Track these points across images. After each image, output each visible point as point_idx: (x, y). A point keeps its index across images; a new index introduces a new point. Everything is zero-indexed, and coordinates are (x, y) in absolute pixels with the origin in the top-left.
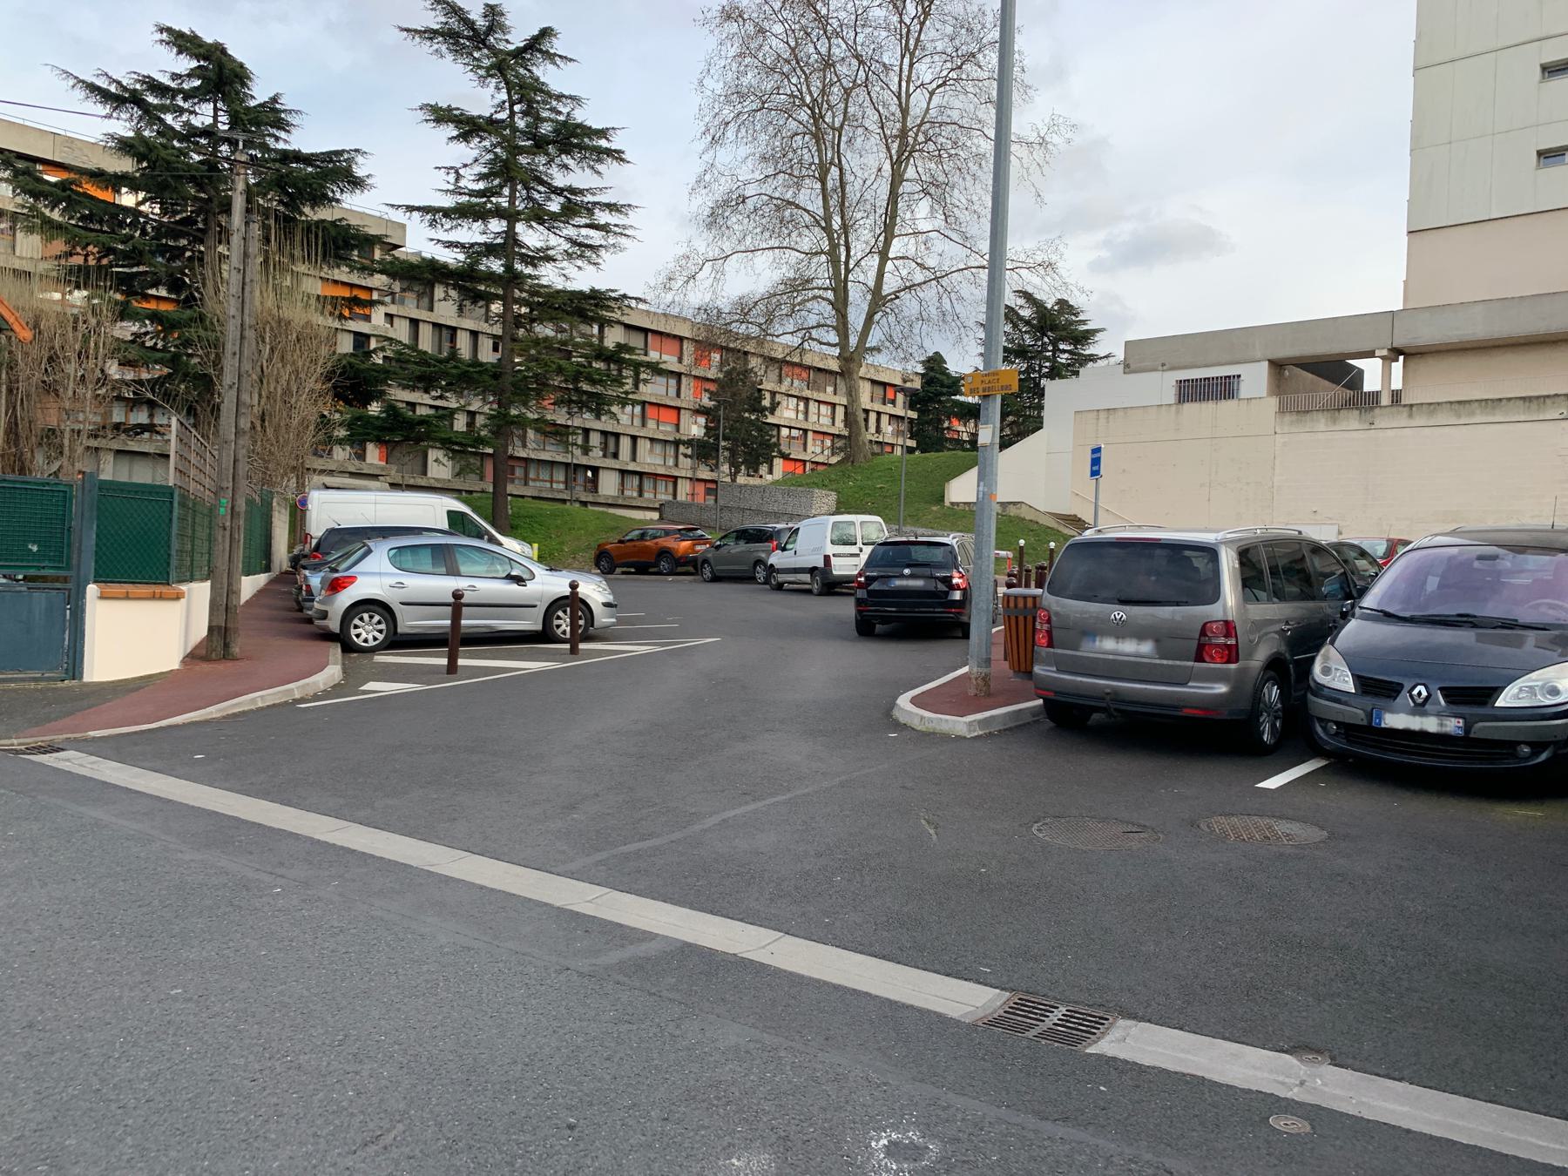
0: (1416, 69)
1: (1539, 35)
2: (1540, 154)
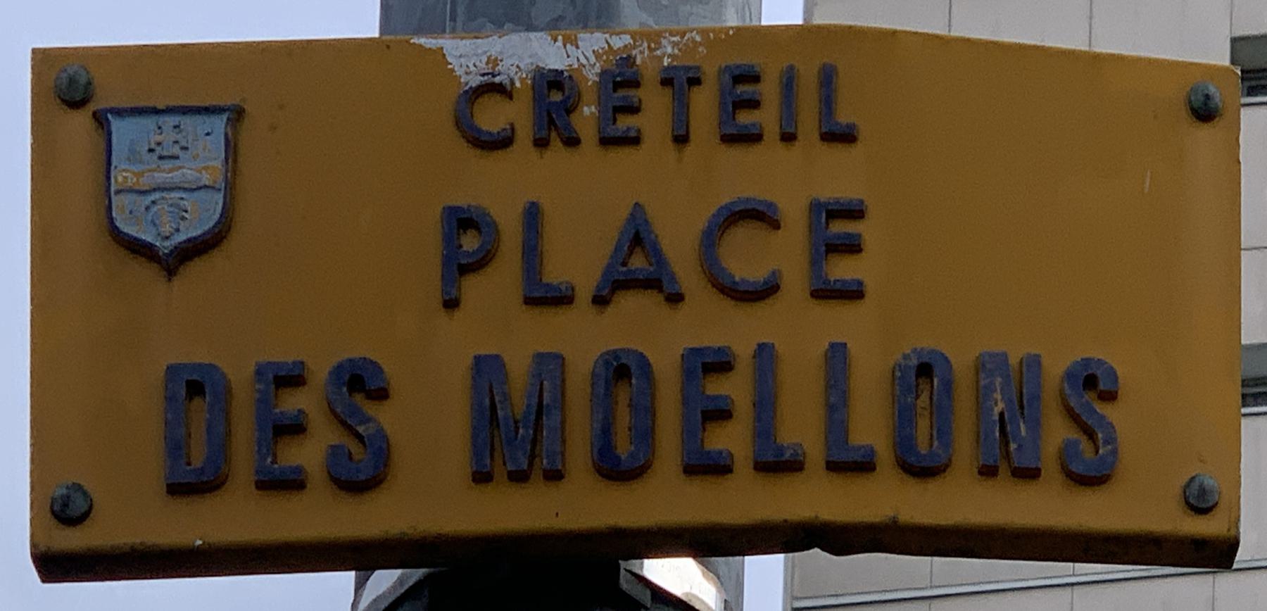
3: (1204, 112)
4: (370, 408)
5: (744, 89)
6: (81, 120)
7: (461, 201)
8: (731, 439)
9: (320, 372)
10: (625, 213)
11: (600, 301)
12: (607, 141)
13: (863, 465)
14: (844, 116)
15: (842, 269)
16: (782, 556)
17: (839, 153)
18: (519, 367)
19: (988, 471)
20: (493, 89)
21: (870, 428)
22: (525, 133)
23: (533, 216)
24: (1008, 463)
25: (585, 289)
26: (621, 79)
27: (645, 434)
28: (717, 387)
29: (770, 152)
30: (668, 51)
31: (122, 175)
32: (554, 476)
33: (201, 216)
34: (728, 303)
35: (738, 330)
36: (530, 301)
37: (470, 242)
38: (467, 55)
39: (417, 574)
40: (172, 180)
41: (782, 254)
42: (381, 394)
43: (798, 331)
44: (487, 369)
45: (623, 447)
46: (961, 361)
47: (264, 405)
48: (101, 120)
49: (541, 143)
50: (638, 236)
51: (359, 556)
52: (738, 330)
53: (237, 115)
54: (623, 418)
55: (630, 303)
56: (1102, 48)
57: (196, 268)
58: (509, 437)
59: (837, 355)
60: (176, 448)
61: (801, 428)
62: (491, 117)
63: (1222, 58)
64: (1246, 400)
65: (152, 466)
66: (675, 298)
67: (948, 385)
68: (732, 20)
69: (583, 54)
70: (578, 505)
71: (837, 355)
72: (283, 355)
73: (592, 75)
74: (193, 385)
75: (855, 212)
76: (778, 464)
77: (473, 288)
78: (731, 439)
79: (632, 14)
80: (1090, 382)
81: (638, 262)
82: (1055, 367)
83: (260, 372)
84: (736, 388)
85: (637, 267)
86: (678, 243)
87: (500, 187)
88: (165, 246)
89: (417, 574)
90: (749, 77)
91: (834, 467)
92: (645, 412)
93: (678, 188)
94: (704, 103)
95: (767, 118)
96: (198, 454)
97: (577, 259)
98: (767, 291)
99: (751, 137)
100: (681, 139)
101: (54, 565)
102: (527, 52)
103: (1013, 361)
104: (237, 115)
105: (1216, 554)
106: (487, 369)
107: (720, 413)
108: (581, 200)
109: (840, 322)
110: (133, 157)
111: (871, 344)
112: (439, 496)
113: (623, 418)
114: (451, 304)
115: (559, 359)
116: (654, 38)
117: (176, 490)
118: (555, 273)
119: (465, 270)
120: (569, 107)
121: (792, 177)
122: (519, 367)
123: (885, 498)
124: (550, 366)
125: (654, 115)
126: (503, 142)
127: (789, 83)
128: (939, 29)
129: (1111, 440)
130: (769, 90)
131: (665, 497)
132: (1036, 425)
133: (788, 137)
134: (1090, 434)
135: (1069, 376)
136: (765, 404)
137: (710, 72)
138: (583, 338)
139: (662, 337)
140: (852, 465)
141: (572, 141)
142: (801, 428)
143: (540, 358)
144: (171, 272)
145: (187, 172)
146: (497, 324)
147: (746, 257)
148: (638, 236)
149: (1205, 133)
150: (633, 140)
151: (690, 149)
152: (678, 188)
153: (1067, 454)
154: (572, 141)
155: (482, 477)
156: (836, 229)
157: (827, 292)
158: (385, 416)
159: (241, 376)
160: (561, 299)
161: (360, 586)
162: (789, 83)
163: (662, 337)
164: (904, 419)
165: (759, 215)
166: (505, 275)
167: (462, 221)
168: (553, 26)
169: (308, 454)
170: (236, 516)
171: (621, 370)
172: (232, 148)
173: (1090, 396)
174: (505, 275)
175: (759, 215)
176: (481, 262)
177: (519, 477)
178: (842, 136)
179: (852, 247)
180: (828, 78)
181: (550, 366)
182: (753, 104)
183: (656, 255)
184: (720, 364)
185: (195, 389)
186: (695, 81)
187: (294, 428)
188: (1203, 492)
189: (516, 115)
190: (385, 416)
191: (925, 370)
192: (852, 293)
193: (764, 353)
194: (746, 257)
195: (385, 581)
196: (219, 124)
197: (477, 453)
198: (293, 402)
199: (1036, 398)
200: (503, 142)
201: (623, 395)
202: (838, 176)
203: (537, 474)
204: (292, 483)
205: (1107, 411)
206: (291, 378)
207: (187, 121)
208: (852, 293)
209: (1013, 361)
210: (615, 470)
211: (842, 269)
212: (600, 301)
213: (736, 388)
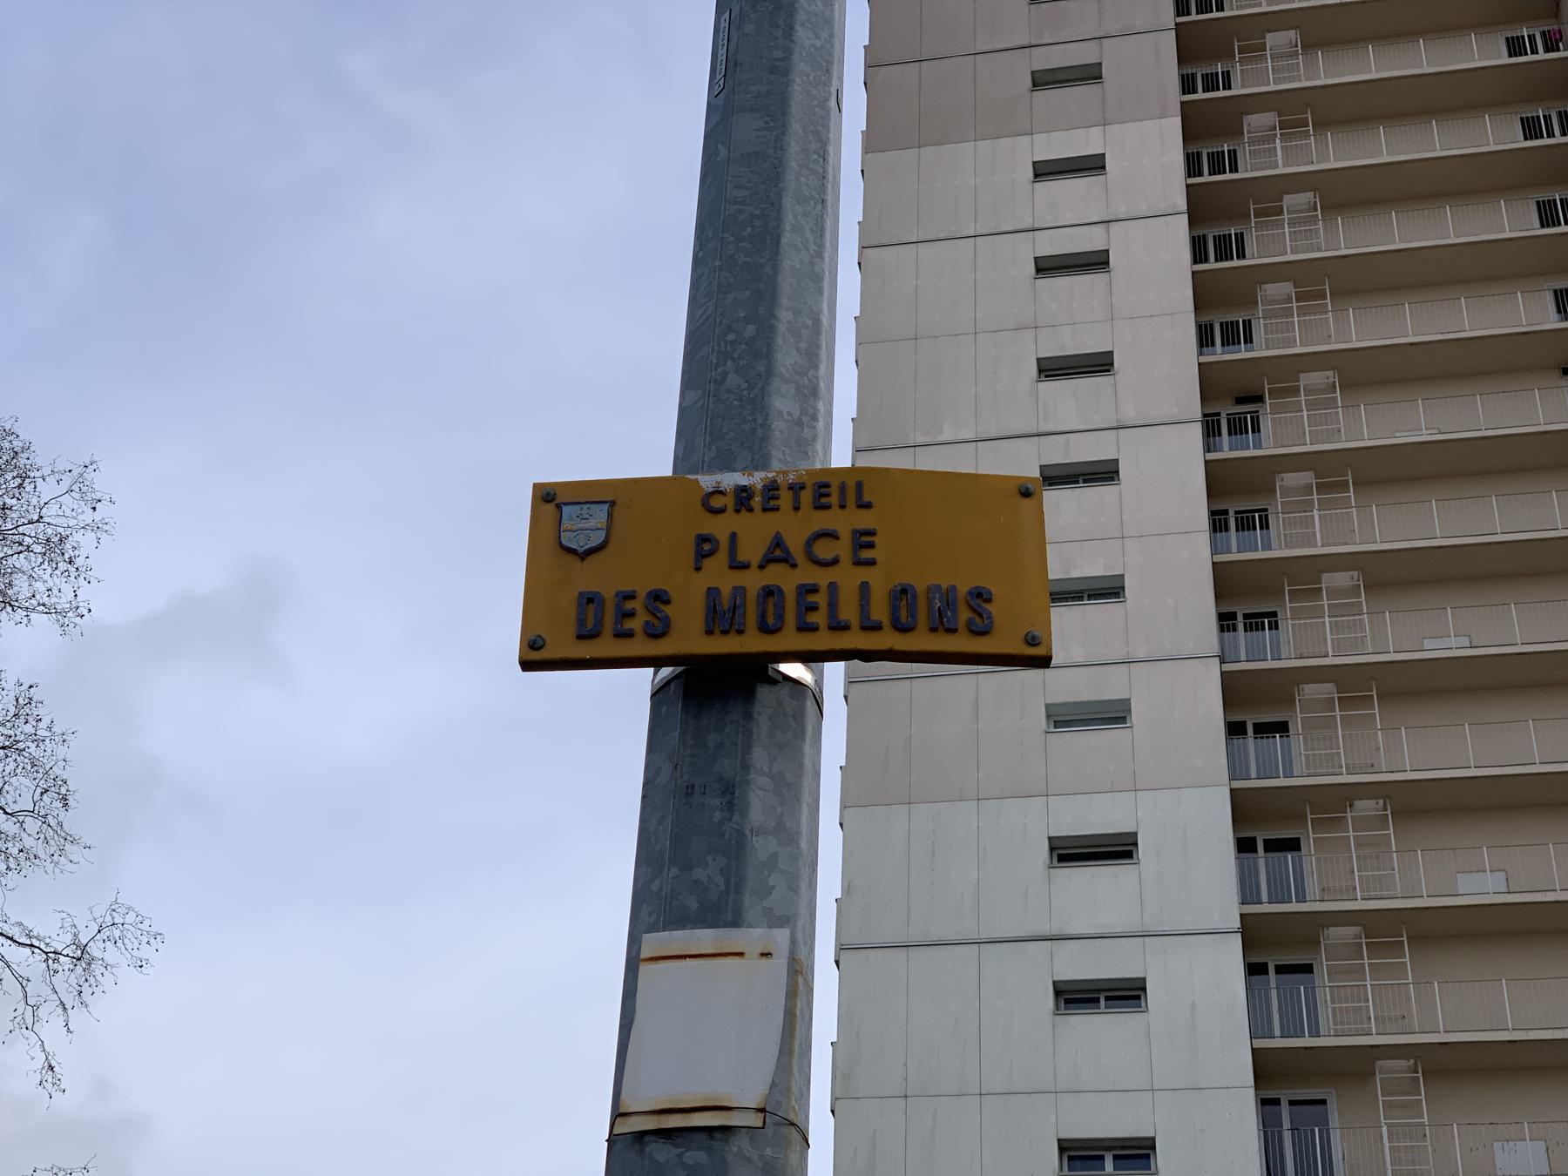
0: (863, 248)
1: (1046, 930)
2: (1064, 1146)
3: (1026, 494)
4: (663, 607)
5: (824, 490)
6: (551, 506)
7: (704, 532)
8: (819, 618)
9: (642, 594)
10: (772, 535)
11: (761, 567)
12: (765, 510)
13: (877, 627)
14: (866, 499)
15: (866, 554)
16: (842, 663)
17: (863, 512)
18: (726, 592)
19: (933, 630)
20: (718, 492)
21: (880, 613)
22: (730, 508)
23: (733, 537)
24: (942, 625)
25: (755, 562)
26: (771, 489)
27: (780, 617)
28: (812, 598)
29: (835, 512)
30: (791, 478)
31: (564, 526)
32: (740, 632)
33: (597, 539)
34: (815, 567)
35: (822, 578)
36: (731, 567)
37: (706, 547)
38: (707, 481)
39: (680, 669)
40: (586, 527)
41: (843, 548)
42: (667, 602)
43: (848, 578)
44: (713, 594)
45: (770, 620)
46: (921, 588)
47: (618, 606)
48: (558, 507)
49: (737, 511)
50: (778, 543)
51: (656, 662)
52: (822, 578)
53: (613, 503)
54: (771, 610)
55: (774, 568)
56: (981, 471)
57: (590, 559)
58: (721, 616)
59: (865, 588)
60: (581, 622)
61: (849, 612)
62: (717, 502)
63: (1037, 474)
64: (1053, 600)
65: (571, 628)
66: (794, 566)
67: (915, 596)
68: (818, 466)
69: (757, 479)
70: (752, 643)
71: (865, 588)
72: (626, 587)
73: (759, 487)
74: (589, 599)
75: (872, 533)
76: (839, 627)
77: (708, 563)
78: (819, 618)
79: (776, 465)
80: (979, 595)
81: (778, 553)
82: (963, 589)
83: (617, 595)
84: (820, 599)
85: (777, 553)
86: (796, 546)
87: (720, 528)
88: (581, 550)
89: (680, 669)
90: (827, 486)
91: (863, 628)
92: (912, 608)
93: (795, 527)
94: (806, 497)
95: (834, 500)
96: (590, 624)
97: (751, 551)
98: (835, 562)
99: (827, 507)
100: (797, 508)
101: (527, 665)
102: (732, 480)
103: (944, 587)
104: (613, 503)
105: (1044, 662)
106: (713, 594)
107: (814, 608)
108: (754, 531)
109: (863, 574)
110: (571, 518)
111: (880, 583)
112: (691, 638)
113: (771, 610)
114: (698, 569)
115: (744, 589)
116: (785, 473)
117: (580, 637)
118: (742, 557)
119: (704, 556)
120: (750, 497)
121: (845, 521)
122: (726, 592)
123: (961, 643)
124: (739, 591)
125: (785, 499)
126: (722, 511)
127: (843, 488)
128: (911, 467)
129: (990, 617)
130: (834, 491)
131: (789, 639)
132: (955, 612)
133: (842, 507)
134: (980, 615)
135: (970, 593)
136: (833, 605)
137: (809, 485)
138: (753, 581)
139: (787, 580)
140: (872, 627)
141: (751, 510)
142: (849, 612)
143: (735, 588)
144: (583, 559)
145: (592, 523)
146: (716, 573)
147: (824, 550)
148: (778, 543)
149: (1027, 502)
150: (777, 509)
151: (800, 513)
152: (795, 527)
153: (969, 623)
154: (751, 510)
155: (709, 632)
156: (863, 539)
157: (858, 563)
158: (668, 610)
159: (609, 594)
160: (746, 566)
161: (655, 673)
162: (843, 488)
163: (787, 580)
164: (894, 610)
165: (832, 535)
166: (722, 557)
167: (703, 539)
168: (743, 470)
169: (636, 624)
170: (606, 646)
171: (769, 592)
172: (610, 515)
173: (979, 601)
174: (722, 557)
175: (832, 535)
176: (711, 553)
177: (725, 632)
178: (868, 506)
179: (871, 546)
180: (859, 485)
181: (739, 591)
182: (828, 495)
183: (786, 550)
184: (814, 589)
185: (590, 601)
186: (803, 488)
187: (631, 614)
188: (1034, 637)
189: (729, 501)
190: (668, 610)
191: (904, 591)
192: (872, 563)
193: (833, 586)
194: (824, 550)
195: (666, 672)
196: (606, 507)
197: (707, 623)
198: (629, 605)
199: (955, 602)
200: (722, 511)
201: (771, 602)
202: (864, 520)
203: (717, 632)
204: (629, 635)
205: (668, 609)
206: (630, 596)
207: (593, 507)
208: (872, 563)
209: (944, 587)
210: (765, 629)
211: (866, 554)
212: (761, 567)
213: (820, 599)
